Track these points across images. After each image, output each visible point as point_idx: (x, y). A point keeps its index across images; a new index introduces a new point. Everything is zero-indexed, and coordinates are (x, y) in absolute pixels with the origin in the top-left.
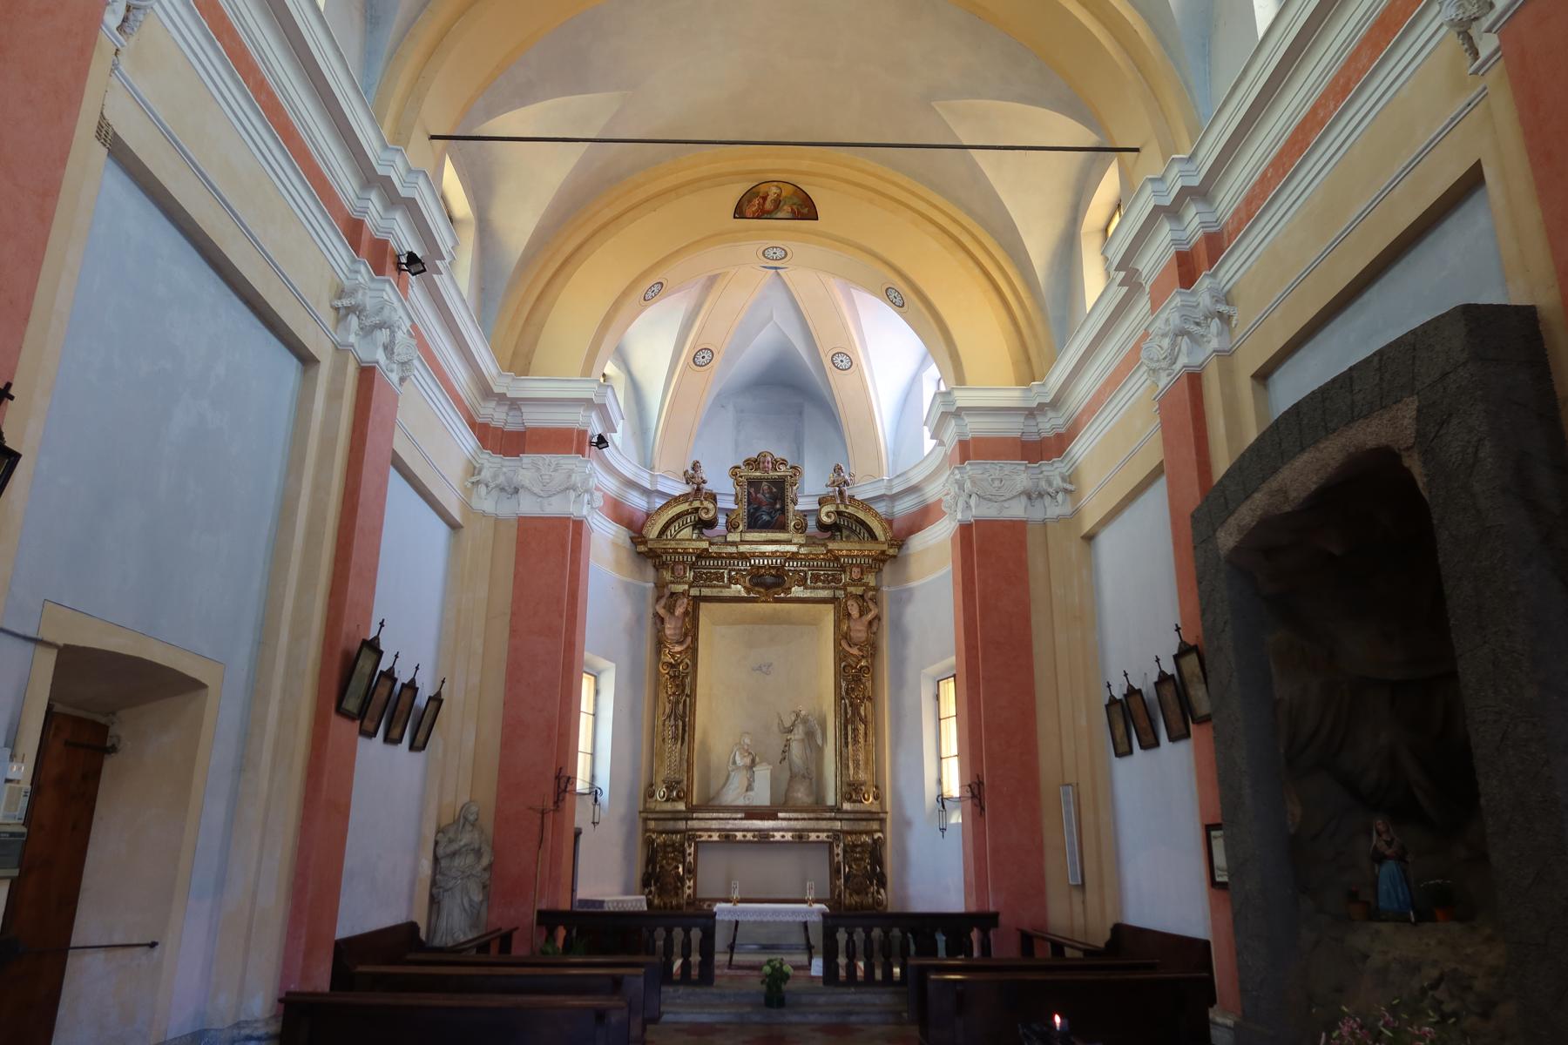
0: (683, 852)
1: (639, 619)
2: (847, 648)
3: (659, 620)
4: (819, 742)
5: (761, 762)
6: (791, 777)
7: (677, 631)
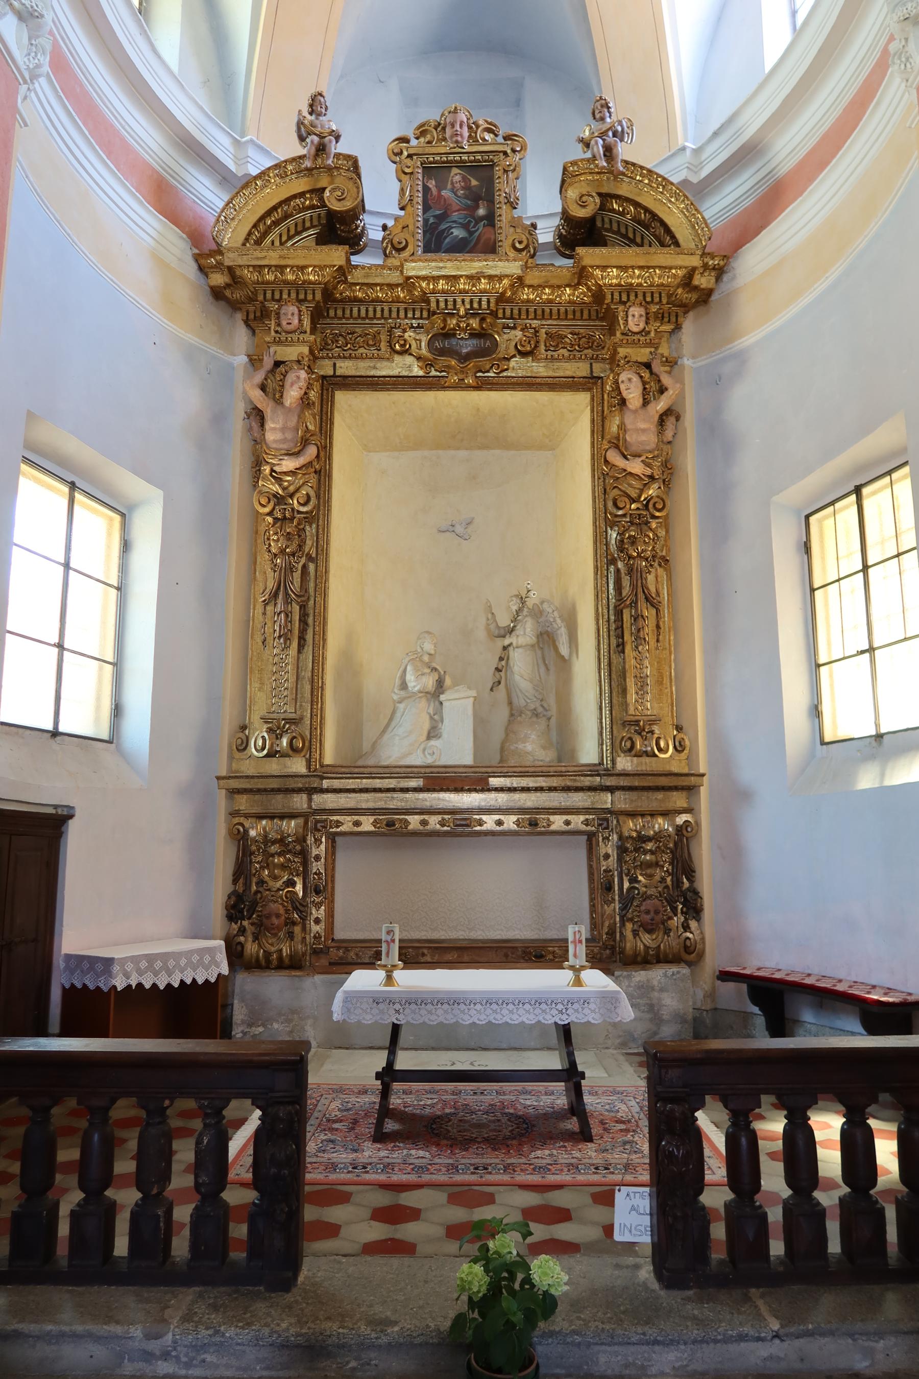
0: (304, 854)
1: (218, 419)
2: (619, 461)
3: (257, 415)
4: (564, 650)
5: (456, 684)
6: (512, 715)
7: (289, 435)
